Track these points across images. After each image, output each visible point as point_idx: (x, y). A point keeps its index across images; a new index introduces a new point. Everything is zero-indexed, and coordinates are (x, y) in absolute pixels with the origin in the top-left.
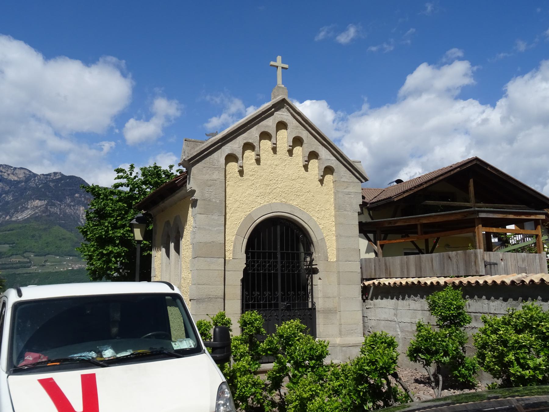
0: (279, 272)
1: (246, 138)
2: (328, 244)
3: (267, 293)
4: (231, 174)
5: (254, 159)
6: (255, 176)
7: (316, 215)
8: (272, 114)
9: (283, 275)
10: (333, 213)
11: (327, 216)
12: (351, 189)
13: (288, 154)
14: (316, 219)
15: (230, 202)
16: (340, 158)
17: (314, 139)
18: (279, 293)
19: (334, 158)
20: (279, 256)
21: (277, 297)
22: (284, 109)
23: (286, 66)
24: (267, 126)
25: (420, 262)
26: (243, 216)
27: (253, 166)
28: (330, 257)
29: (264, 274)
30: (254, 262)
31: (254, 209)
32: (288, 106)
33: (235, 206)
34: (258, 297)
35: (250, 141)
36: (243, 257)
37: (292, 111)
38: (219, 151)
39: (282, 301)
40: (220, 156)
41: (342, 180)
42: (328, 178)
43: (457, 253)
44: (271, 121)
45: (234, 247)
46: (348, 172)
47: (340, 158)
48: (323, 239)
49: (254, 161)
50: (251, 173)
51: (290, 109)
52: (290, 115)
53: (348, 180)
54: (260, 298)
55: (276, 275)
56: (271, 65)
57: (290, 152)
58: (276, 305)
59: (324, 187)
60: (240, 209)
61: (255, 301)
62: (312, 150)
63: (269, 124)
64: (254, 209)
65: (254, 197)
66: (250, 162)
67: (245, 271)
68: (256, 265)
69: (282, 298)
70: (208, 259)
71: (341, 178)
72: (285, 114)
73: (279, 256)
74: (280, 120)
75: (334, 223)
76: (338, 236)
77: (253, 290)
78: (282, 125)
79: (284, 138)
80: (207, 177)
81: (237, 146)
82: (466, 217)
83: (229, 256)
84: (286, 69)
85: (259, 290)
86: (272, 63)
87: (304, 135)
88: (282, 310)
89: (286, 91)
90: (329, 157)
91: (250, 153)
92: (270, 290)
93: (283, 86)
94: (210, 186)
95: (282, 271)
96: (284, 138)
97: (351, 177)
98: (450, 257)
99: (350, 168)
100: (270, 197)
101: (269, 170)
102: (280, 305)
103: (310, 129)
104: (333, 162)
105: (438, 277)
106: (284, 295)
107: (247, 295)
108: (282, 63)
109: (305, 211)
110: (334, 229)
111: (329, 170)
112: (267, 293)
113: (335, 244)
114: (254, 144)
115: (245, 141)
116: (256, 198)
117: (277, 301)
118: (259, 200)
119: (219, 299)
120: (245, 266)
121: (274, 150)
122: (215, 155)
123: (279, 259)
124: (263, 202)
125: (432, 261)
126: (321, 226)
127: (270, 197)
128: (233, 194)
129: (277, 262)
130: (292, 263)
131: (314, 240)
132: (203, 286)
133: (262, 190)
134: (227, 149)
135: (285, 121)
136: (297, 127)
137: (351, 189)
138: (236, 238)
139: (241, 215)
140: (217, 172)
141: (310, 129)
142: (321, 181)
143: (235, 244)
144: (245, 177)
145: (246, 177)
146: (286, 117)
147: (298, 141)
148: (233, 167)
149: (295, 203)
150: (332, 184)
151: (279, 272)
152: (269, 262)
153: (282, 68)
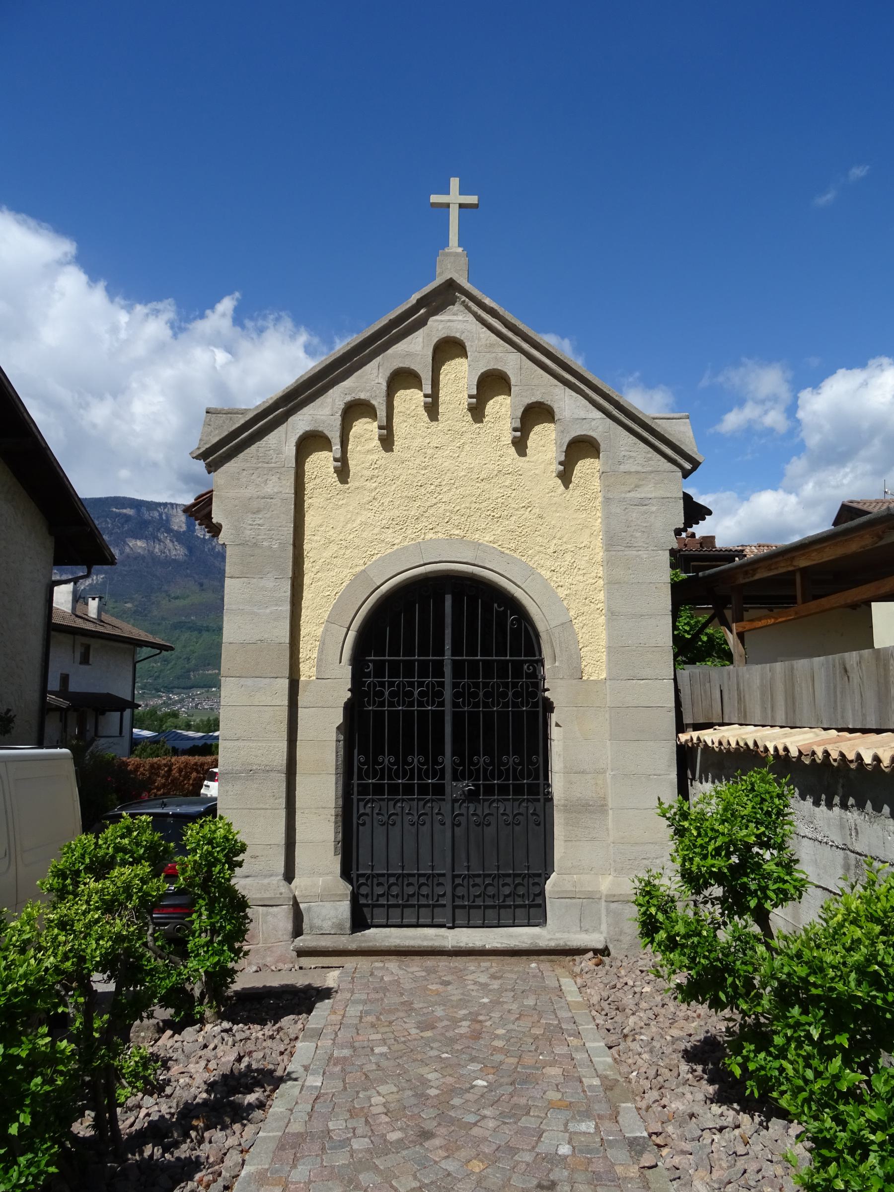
0: (448, 709)
1: (351, 390)
2: (583, 636)
3: (416, 760)
4: (318, 481)
5: (377, 437)
6: (379, 480)
7: (548, 563)
8: (422, 323)
9: (457, 718)
10: (600, 555)
11: (582, 564)
12: (648, 491)
13: (469, 417)
14: (546, 574)
15: (314, 545)
16: (616, 413)
17: (542, 372)
18: (448, 759)
19: (599, 415)
20: (448, 670)
21: (443, 770)
22: (457, 307)
23: (473, 199)
24: (409, 355)
25: (793, 685)
26: (347, 575)
27: (375, 457)
28: (587, 670)
29: (474, 716)
30: (382, 684)
31: (375, 558)
32: (464, 298)
33: (327, 554)
34: (515, 770)
35: (363, 396)
36: (345, 672)
37: (475, 308)
38: (282, 429)
39: (455, 778)
40: (282, 441)
41: (622, 468)
42: (585, 467)
43: (861, 657)
44: (420, 340)
45: (321, 651)
46: (642, 445)
47: (616, 413)
48: (568, 624)
49: (376, 442)
50: (368, 473)
51: (471, 304)
52: (471, 318)
53: (639, 469)
54: (522, 770)
55: (439, 717)
56: (434, 205)
57: (477, 412)
58: (439, 790)
59: (574, 494)
60: (338, 561)
61: (507, 779)
62: (534, 400)
63: (415, 349)
64: (375, 558)
65: (377, 530)
66: (367, 447)
67: (350, 708)
68: (416, 693)
69: (455, 771)
70: (249, 682)
71: (620, 463)
72: (460, 318)
73: (448, 670)
74: (442, 334)
75: (601, 582)
76: (612, 615)
77: (409, 751)
78: (449, 348)
79: (459, 379)
80: (251, 491)
81: (327, 411)
82: (881, 538)
83: (307, 671)
84: (475, 206)
85: (517, 751)
86: (435, 199)
87: (512, 363)
88: (455, 801)
89: (464, 260)
90: (582, 414)
91: (366, 426)
92: (423, 751)
93: (460, 250)
94: (259, 511)
95: (455, 705)
96: (459, 379)
97: (650, 459)
98: (846, 671)
99: (646, 434)
100: (419, 527)
101: (418, 461)
102: (448, 789)
103: (525, 346)
104: (595, 423)
105: (825, 729)
106: (462, 763)
107: (364, 764)
108: (461, 193)
109: (517, 555)
110: (601, 596)
111: (581, 448)
112: (416, 760)
113: (604, 636)
114: (374, 402)
115: (349, 398)
116: (380, 533)
117: (442, 777)
118: (389, 535)
119: (273, 774)
120: (349, 694)
121: (432, 409)
122: (272, 438)
123: (448, 679)
124: (397, 539)
125: (813, 681)
126: (562, 593)
127: (419, 527)
128: (321, 526)
129: (442, 685)
130: (515, 685)
131: (541, 626)
132: (236, 743)
133: (397, 513)
134: (302, 422)
135: (458, 335)
136: (492, 345)
137: (648, 491)
138: (326, 630)
139: (342, 576)
140: (275, 478)
141: (525, 346)
142: (565, 477)
143: (323, 643)
144: (353, 483)
145: (357, 484)
146: (460, 326)
147: (492, 383)
148: (322, 463)
149: (487, 538)
150: (596, 484)
151: (448, 709)
152: (421, 684)
153: (461, 206)
